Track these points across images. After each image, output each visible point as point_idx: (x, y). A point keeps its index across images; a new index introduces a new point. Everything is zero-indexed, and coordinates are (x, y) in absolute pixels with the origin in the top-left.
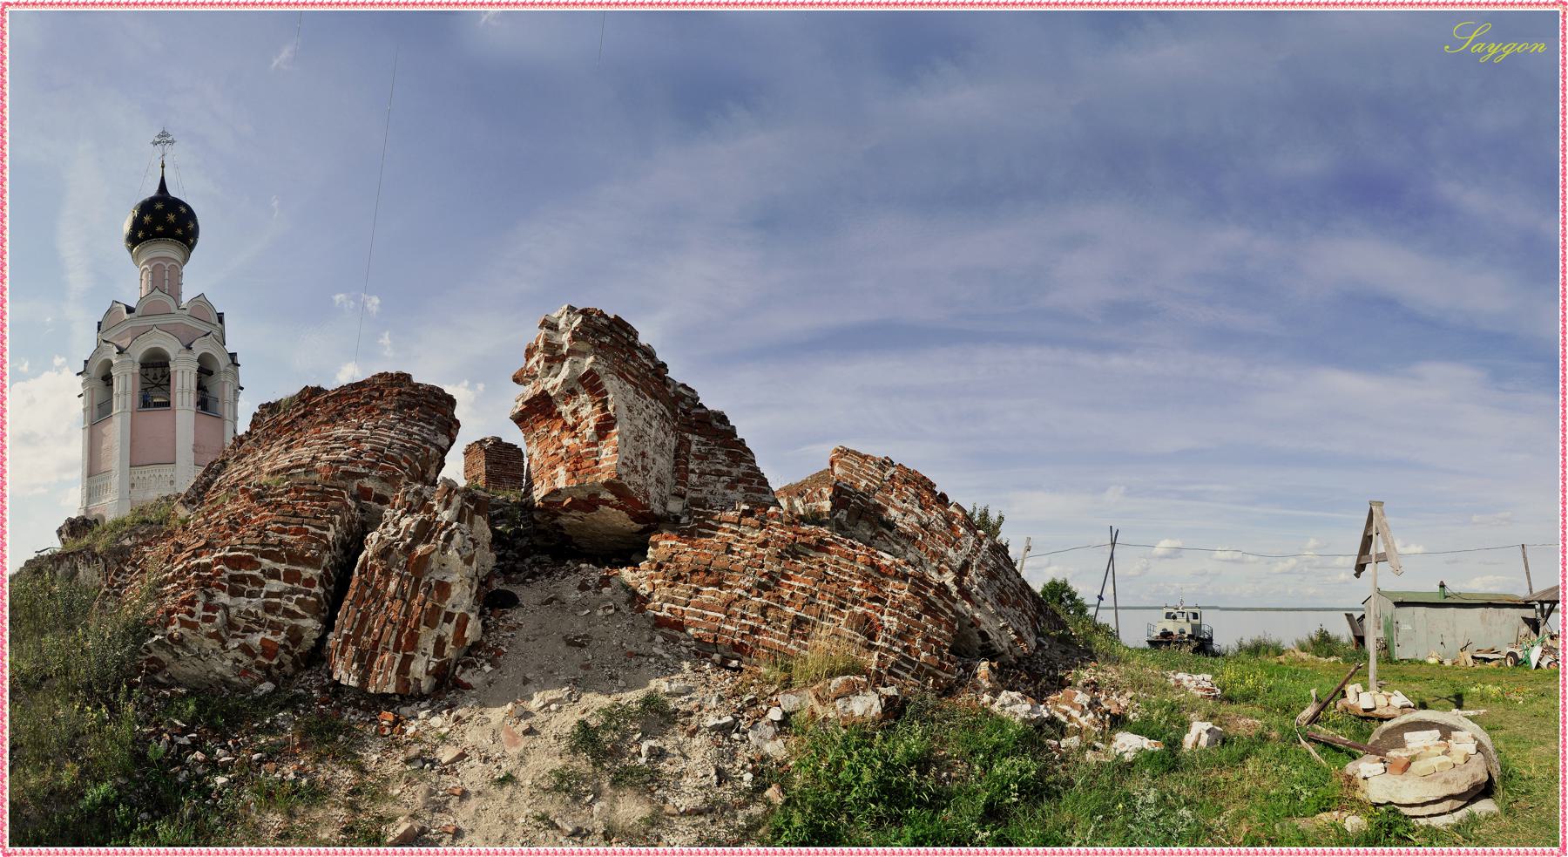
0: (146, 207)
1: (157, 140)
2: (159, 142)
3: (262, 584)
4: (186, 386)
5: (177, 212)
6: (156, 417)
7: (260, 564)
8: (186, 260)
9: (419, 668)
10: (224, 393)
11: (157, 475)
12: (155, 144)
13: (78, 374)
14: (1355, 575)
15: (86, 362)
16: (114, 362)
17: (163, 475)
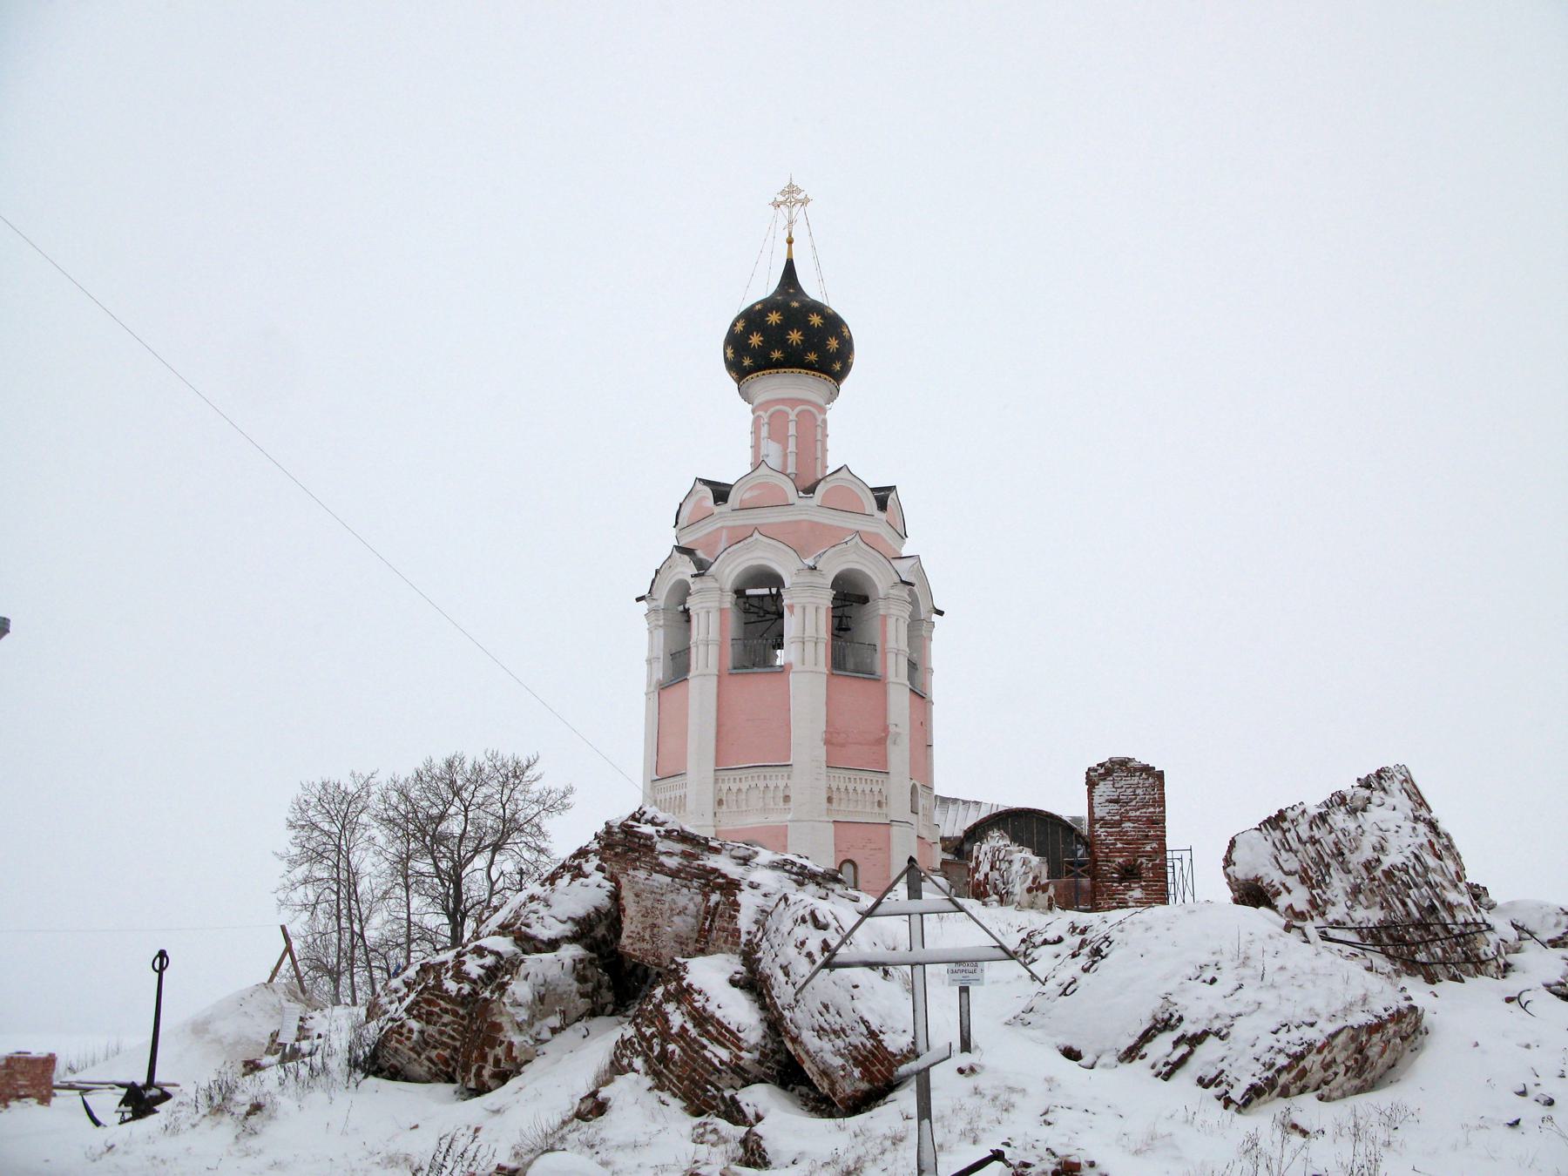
0: (752, 318)
1: (781, 198)
2: (783, 203)
3: (441, 1017)
5: (806, 328)
6: (755, 685)
7: (439, 1005)
8: (833, 395)
10: (884, 633)
11: (762, 784)
12: (777, 205)
13: (638, 600)
14: (883, 978)
17: (772, 784)
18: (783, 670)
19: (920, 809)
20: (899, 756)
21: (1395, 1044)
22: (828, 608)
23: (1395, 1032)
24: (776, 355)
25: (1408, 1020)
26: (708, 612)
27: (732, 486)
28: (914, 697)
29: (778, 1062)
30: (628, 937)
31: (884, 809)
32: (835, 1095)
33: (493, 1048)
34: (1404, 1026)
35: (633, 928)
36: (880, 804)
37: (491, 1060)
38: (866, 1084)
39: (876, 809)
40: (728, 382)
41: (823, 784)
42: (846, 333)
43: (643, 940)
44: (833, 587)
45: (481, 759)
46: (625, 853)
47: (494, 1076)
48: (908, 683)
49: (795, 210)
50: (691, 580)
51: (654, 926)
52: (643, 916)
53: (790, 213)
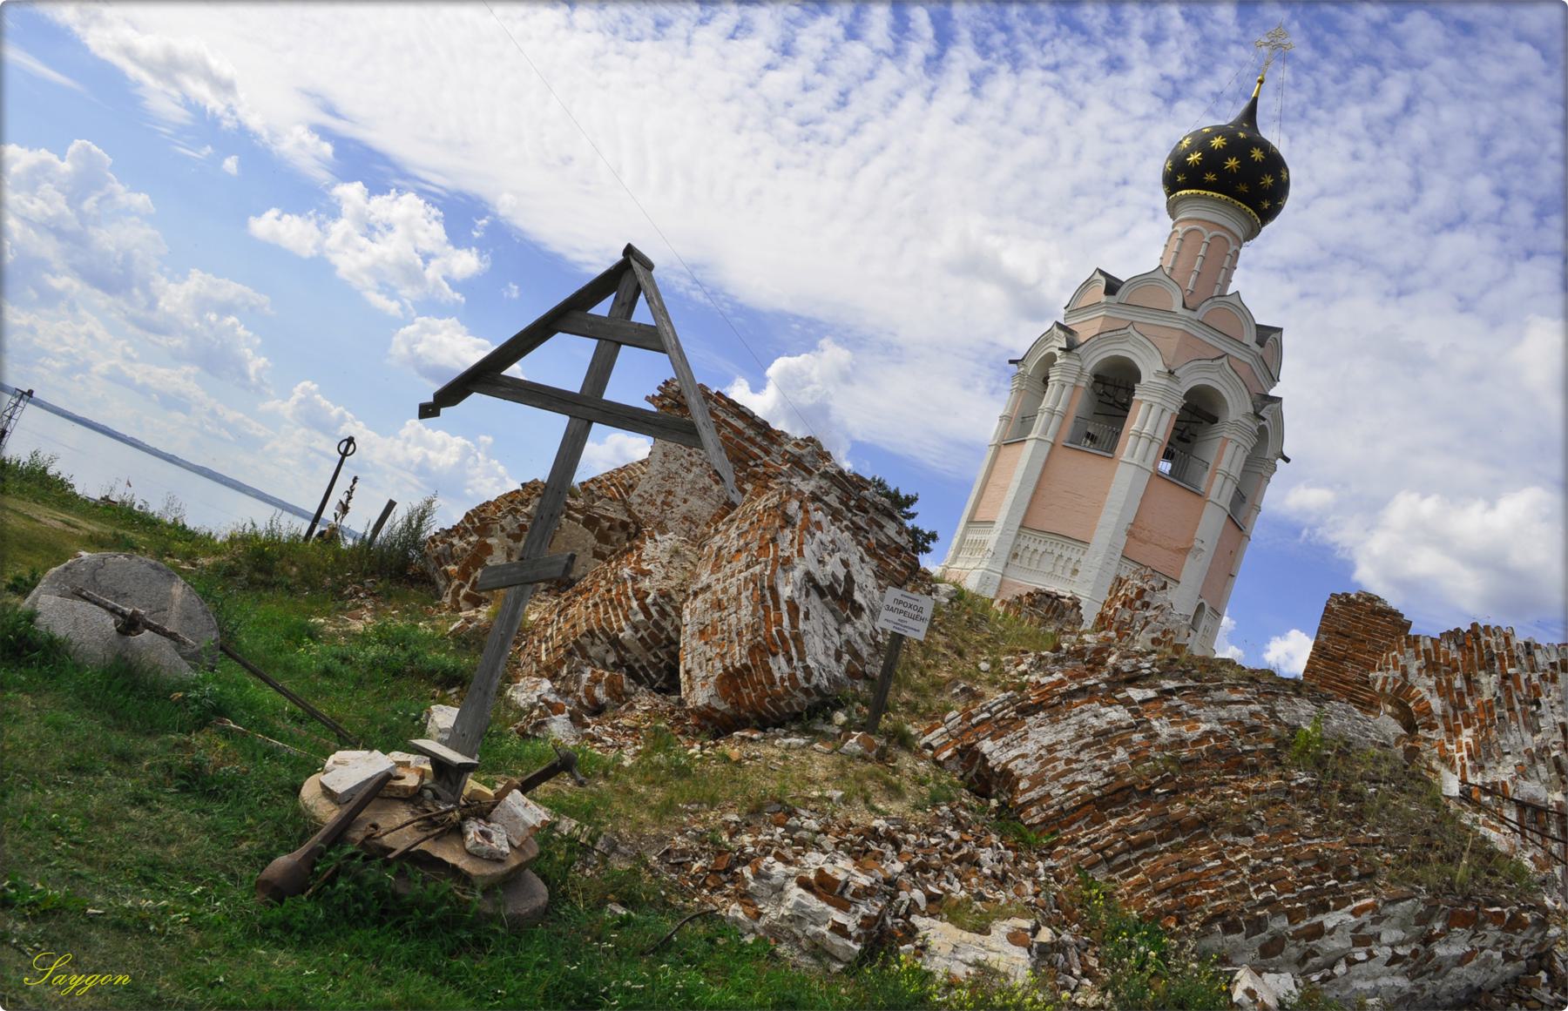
4: (1147, 429)
8: (1253, 233)
11: (1057, 552)
13: (1011, 362)
19: (1202, 627)
21: (1489, 957)
22: (1173, 414)
23: (1498, 941)
24: (1210, 177)
25: (1526, 935)
26: (1064, 386)
27: (1122, 283)
28: (1230, 522)
30: (640, 496)
34: (1518, 940)
35: (647, 488)
38: (728, 706)
40: (1161, 198)
42: (1285, 176)
43: (654, 504)
44: (1185, 397)
46: (672, 406)
47: (467, 597)
48: (1228, 509)
52: (663, 479)
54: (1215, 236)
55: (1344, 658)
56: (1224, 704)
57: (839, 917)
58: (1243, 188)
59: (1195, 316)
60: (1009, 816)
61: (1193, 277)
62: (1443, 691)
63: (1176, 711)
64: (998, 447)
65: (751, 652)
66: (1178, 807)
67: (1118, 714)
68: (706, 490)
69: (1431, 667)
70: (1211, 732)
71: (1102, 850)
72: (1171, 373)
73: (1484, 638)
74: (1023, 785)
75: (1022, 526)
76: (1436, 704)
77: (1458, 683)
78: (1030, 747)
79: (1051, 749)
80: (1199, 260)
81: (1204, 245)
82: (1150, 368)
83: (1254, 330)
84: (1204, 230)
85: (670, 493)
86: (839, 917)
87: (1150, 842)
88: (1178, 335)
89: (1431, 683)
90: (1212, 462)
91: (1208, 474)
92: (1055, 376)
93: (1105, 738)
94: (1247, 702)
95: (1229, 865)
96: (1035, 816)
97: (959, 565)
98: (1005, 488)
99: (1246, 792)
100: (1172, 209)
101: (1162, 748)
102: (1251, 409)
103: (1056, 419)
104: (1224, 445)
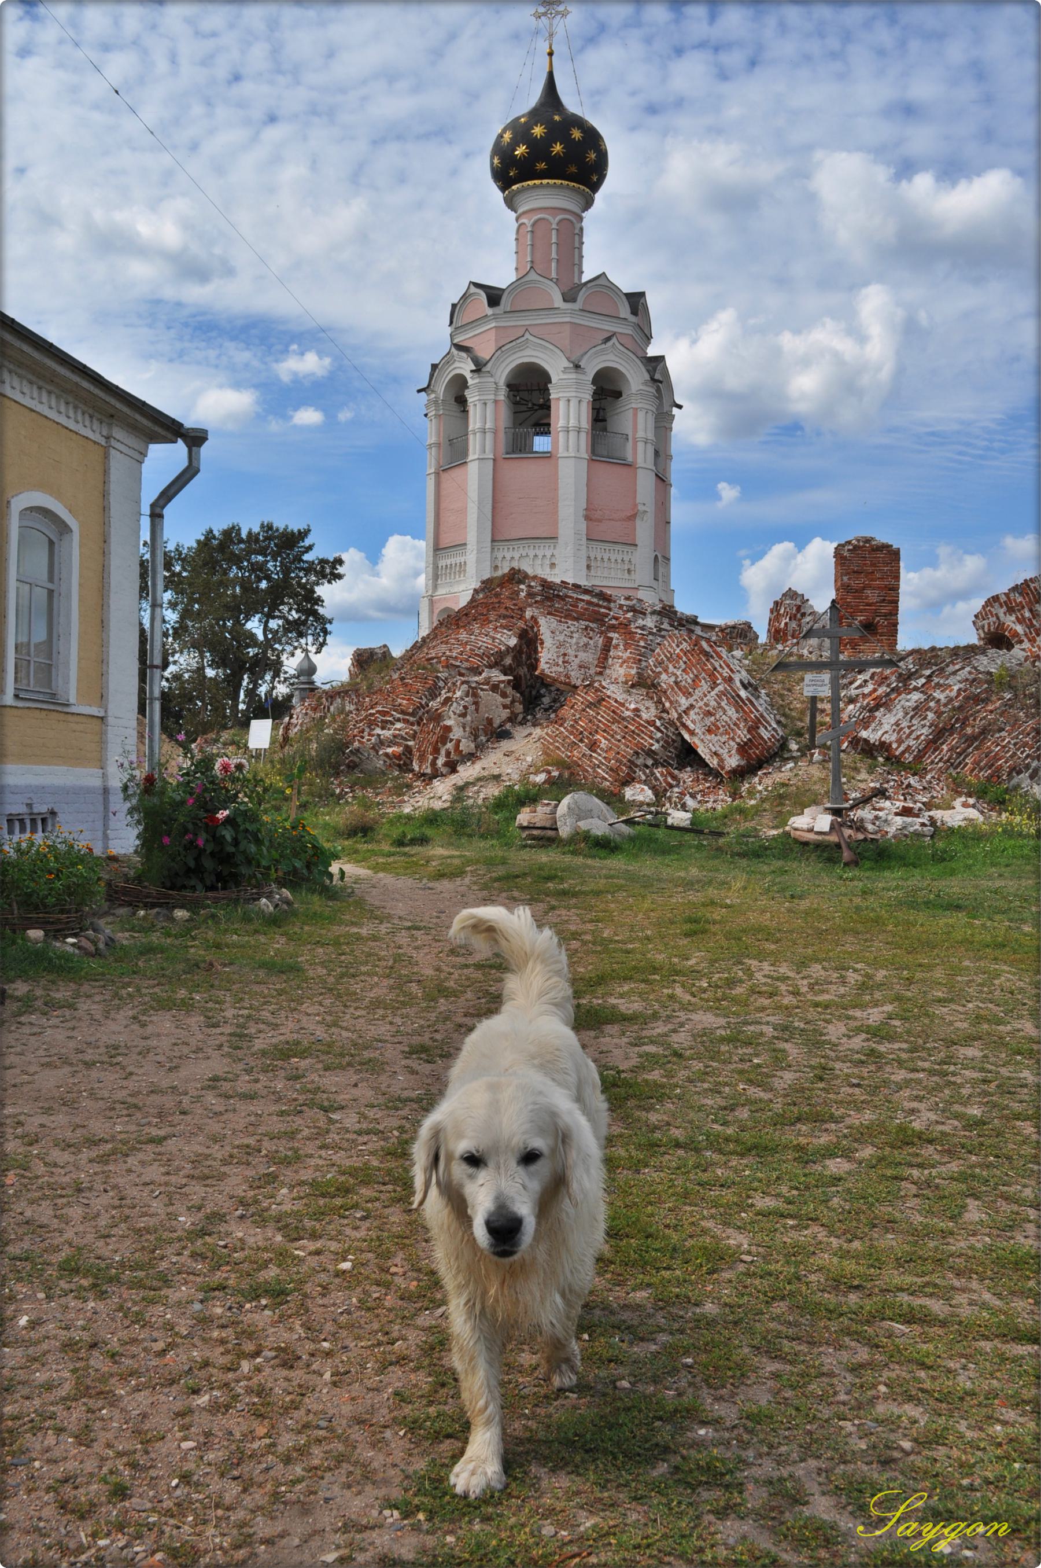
4: (573, 422)
5: (567, 140)
8: (588, 203)
9: (440, 762)
11: (531, 553)
13: (419, 391)
15: (434, 367)
16: (470, 382)
17: (540, 554)
18: (547, 456)
20: (644, 531)
29: (676, 748)
31: (633, 576)
32: (723, 768)
33: (444, 744)
36: (629, 571)
37: (443, 752)
39: (626, 576)
40: (496, 195)
41: (584, 553)
45: (256, 529)
47: (446, 764)
49: (555, 22)
50: (468, 375)
51: (565, 655)
53: (551, 25)
54: (561, 221)
55: (864, 588)
56: (955, 673)
57: (921, 820)
58: (573, 169)
59: (577, 306)
60: (894, 762)
61: (554, 265)
62: (1020, 621)
63: (938, 685)
64: (437, 474)
65: (749, 731)
66: (969, 730)
67: (916, 696)
68: (586, 645)
69: (1010, 610)
70: (959, 690)
71: (948, 761)
72: (577, 366)
73: (1032, 586)
74: (894, 746)
75: (493, 541)
76: (1019, 629)
77: (1027, 614)
78: (886, 727)
79: (897, 724)
80: (554, 247)
81: (554, 232)
82: (556, 366)
83: (624, 298)
84: (550, 218)
85: (565, 655)
86: (921, 820)
87: (964, 751)
88: (567, 327)
89: (1013, 618)
90: (630, 432)
91: (630, 444)
92: (472, 397)
93: (919, 710)
94: (963, 668)
95: (1004, 747)
96: (909, 758)
97: (441, 591)
98: (464, 511)
99: (991, 712)
100: (510, 203)
101: (945, 705)
102: (647, 377)
103: (489, 437)
104: (635, 415)
